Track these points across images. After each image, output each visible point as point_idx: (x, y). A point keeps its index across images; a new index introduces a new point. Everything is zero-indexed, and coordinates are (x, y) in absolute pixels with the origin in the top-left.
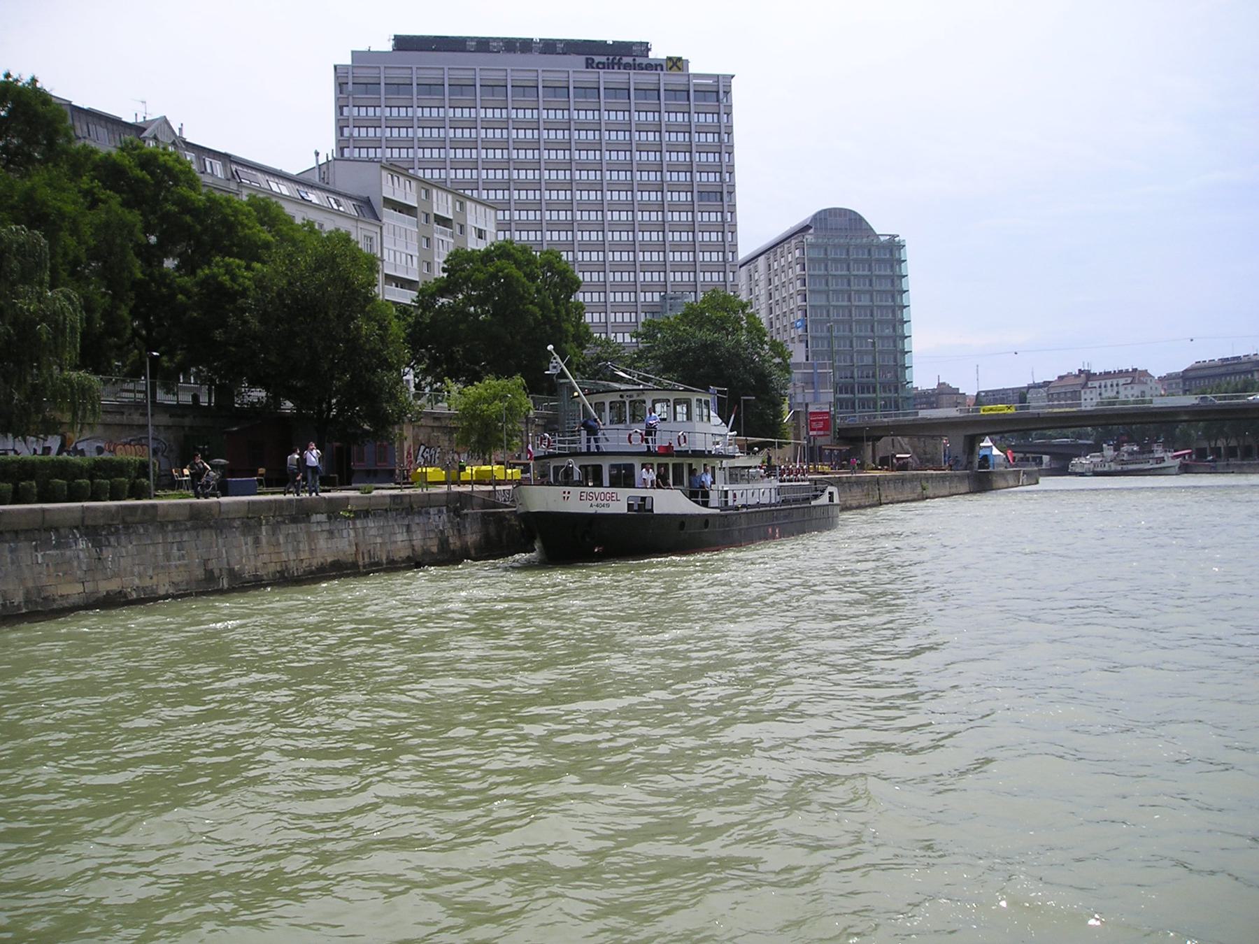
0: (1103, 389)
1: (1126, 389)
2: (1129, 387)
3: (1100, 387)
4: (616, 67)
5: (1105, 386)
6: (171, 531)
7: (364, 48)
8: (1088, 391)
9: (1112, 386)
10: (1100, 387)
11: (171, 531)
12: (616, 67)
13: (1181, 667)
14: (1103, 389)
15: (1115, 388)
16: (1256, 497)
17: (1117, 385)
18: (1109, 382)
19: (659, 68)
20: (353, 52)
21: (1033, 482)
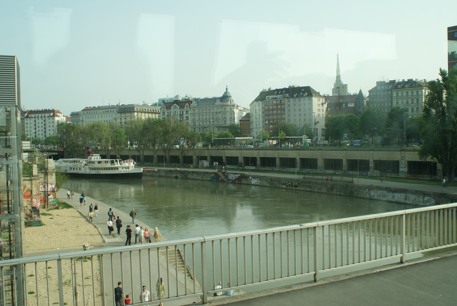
0: (37, 119)
1: (49, 119)
2: (51, 118)
3: (35, 117)
4: (283, 116)
5: (38, 117)
6: (434, 95)
7: (379, 81)
8: (28, 119)
9: (41, 117)
10: (35, 117)
11: (434, 95)
12: (283, 116)
13: (182, 253)
14: (37, 119)
15: (44, 119)
16: (75, 305)
17: (44, 117)
18: (40, 115)
19: (76, 162)
20: (377, 82)
21: (69, 157)
